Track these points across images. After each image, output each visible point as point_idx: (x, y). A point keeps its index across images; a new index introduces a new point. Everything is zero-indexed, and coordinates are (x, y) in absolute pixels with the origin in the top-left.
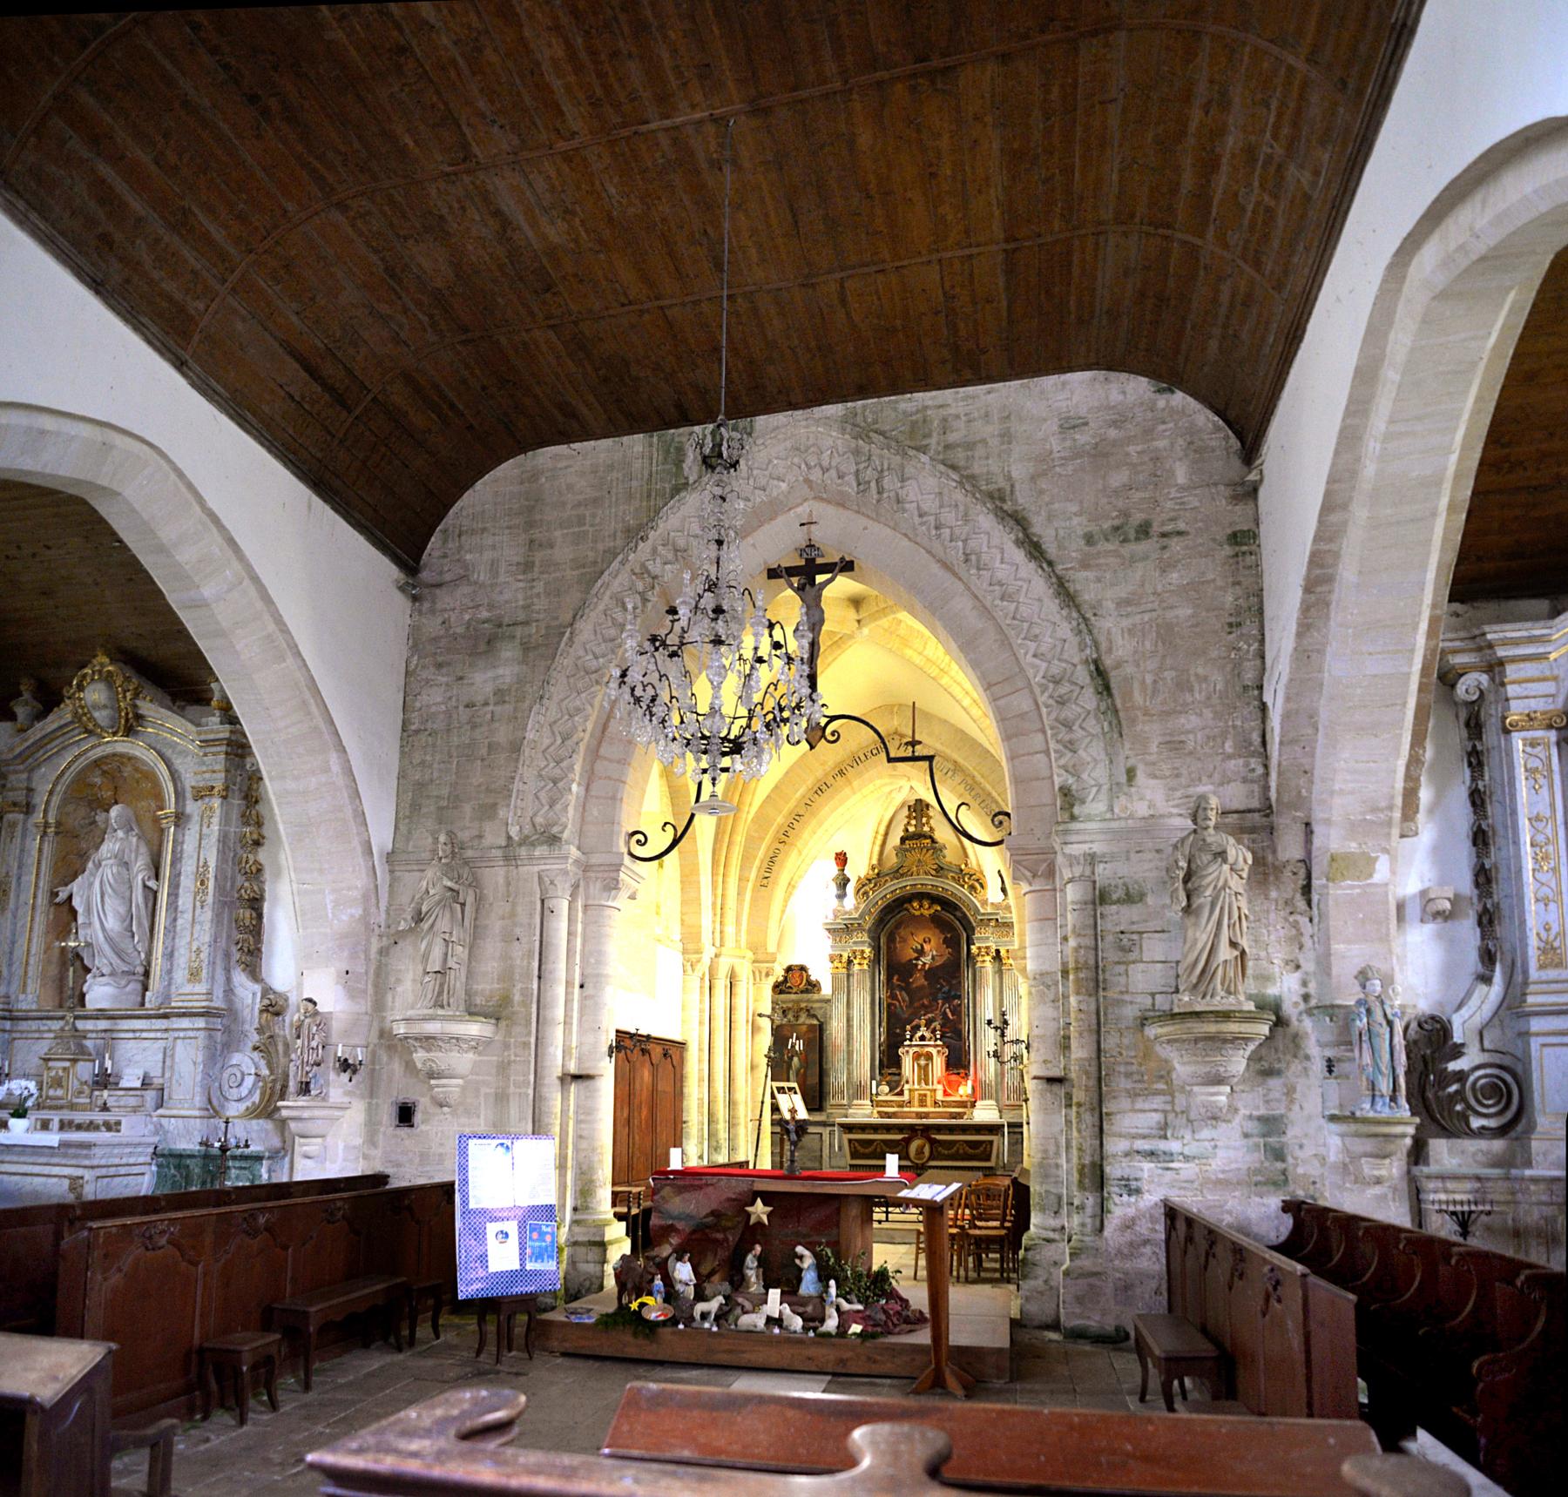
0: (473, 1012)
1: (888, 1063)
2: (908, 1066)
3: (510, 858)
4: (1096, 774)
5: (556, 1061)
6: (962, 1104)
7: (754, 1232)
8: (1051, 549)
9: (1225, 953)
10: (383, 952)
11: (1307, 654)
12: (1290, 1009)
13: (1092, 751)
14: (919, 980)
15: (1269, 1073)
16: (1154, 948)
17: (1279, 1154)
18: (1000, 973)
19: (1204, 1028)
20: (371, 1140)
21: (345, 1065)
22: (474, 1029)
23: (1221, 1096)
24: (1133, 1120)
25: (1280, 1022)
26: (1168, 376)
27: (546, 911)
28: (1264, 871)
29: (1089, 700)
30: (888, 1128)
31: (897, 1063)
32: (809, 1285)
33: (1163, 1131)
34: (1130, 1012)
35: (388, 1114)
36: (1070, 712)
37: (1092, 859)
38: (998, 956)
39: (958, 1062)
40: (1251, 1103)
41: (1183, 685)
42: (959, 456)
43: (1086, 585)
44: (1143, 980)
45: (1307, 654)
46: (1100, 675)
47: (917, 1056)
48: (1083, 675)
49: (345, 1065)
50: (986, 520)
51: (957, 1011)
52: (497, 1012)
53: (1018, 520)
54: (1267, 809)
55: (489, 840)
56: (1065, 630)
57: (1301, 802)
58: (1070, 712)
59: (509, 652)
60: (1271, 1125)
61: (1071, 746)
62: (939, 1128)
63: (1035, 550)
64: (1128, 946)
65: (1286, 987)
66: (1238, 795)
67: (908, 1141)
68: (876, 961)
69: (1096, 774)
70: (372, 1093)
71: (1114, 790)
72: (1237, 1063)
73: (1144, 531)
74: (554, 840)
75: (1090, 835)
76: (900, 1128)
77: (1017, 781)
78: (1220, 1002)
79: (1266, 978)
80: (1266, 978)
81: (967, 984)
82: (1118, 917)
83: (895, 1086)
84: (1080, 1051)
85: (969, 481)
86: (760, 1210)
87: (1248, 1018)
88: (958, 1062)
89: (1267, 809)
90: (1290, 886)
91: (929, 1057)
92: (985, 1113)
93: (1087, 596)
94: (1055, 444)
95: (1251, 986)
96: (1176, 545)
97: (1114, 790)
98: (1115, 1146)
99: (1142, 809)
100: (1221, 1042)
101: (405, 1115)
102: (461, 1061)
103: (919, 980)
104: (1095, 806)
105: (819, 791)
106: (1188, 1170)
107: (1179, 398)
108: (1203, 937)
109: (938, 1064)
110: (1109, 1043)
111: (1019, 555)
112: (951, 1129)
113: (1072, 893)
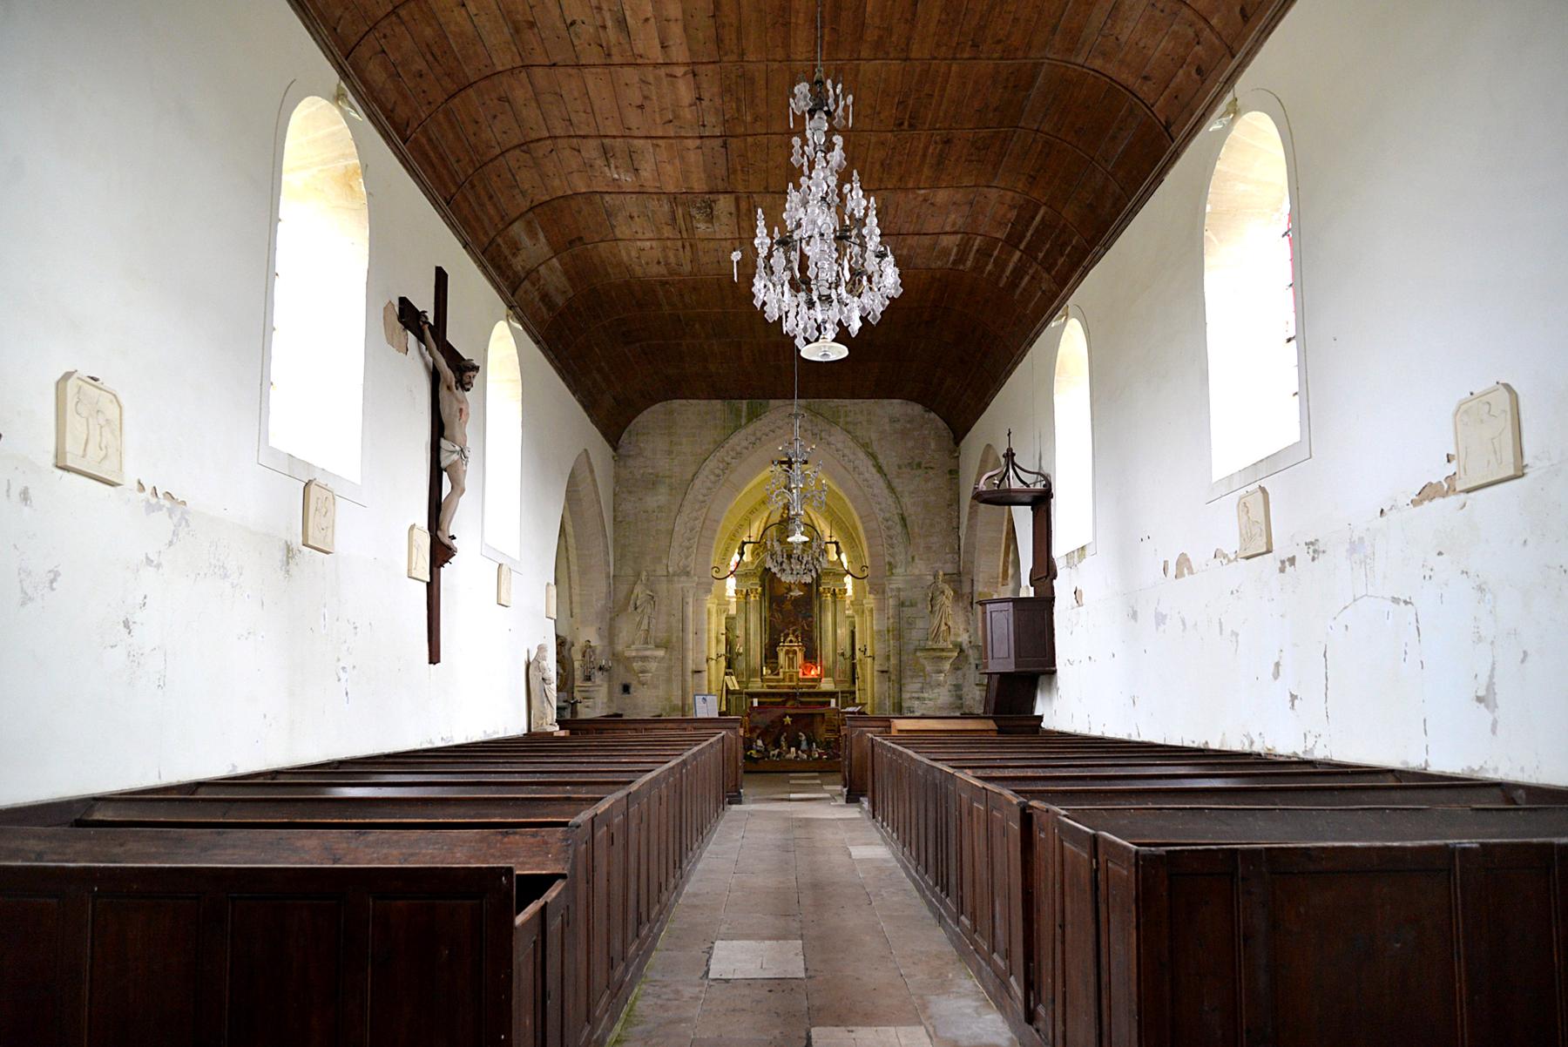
0: (657, 646)
1: (770, 656)
2: (782, 658)
3: (670, 581)
4: (901, 557)
5: (690, 666)
6: (812, 680)
7: (784, 727)
8: (885, 469)
9: (943, 627)
10: (612, 619)
11: (971, 527)
12: (965, 646)
13: (899, 549)
14: (788, 606)
15: (958, 669)
16: (920, 624)
17: (960, 698)
18: (835, 602)
19: (937, 655)
20: (610, 699)
21: (601, 669)
22: (661, 653)
23: (941, 677)
24: (912, 687)
25: (962, 651)
26: (929, 407)
27: (684, 603)
28: (958, 596)
29: (899, 528)
30: (773, 695)
31: (776, 657)
32: (804, 746)
33: (922, 690)
34: (912, 647)
35: (618, 689)
36: (893, 532)
37: (899, 590)
38: (834, 594)
39: (811, 656)
40: (951, 680)
41: (932, 525)
42: (851, 428)
43: (896, 482)
44: (915, 635)
45: (971, 527)
46: (903, 519)
47: (787, 653)
48: (897, 519)
49: (601, 669)
50: (862, 455)
51: (810, 625)
52: (666, 645)
53: (873, 456)
54: (959, 574)
55: (659, 573)
56: (890, 501)
57: (970, 572)
58: (893, 532)
59: (663, 489)
60: (958, 687)
61: (892, 546)
62: (803, 694)
63: (880, 469)
64: (911, 624)
65: (964, 638)
66: (950, 568)
67: (784, 703)
68: (763, 594)
69: (901, 557)
70: (610, 680)
71: (907, 563)
72: (947, 666)
73: (919, 465)
74: (688, 574)
75: (898, 582)
76: (780, 695)
77: (871, 555)
78: (941, 645)
79: (957, 635)
80: (957, 635)
81: (816, 610)
82: (908, 612)
83: (775, 671)
84: (893, 661)
85: (855, 438)
86: (788, 719)
87: (951, 650)
88: (811, 656)
89: (959, 574)
90: (967, 602)
91: (795, 653)
92: (827, 685)
93: (899, 489)
94: (887, 427)
95: (952, 638)
96: (931, 472)
97: (907, 563)
98: (906, 696)
99: (917, 572)
100: (941, 658)
101: (626, 689)
102: (653, 666)
103: (788, 606)
104: (899, 570)
105: (752, 512)
106: (930, 704)
107: (933, 415)
108: (936, 622)
109: (800, 656)
110: (904, 658)
111: (874, 470)
112: (809, 695)
113: (891, 602)
